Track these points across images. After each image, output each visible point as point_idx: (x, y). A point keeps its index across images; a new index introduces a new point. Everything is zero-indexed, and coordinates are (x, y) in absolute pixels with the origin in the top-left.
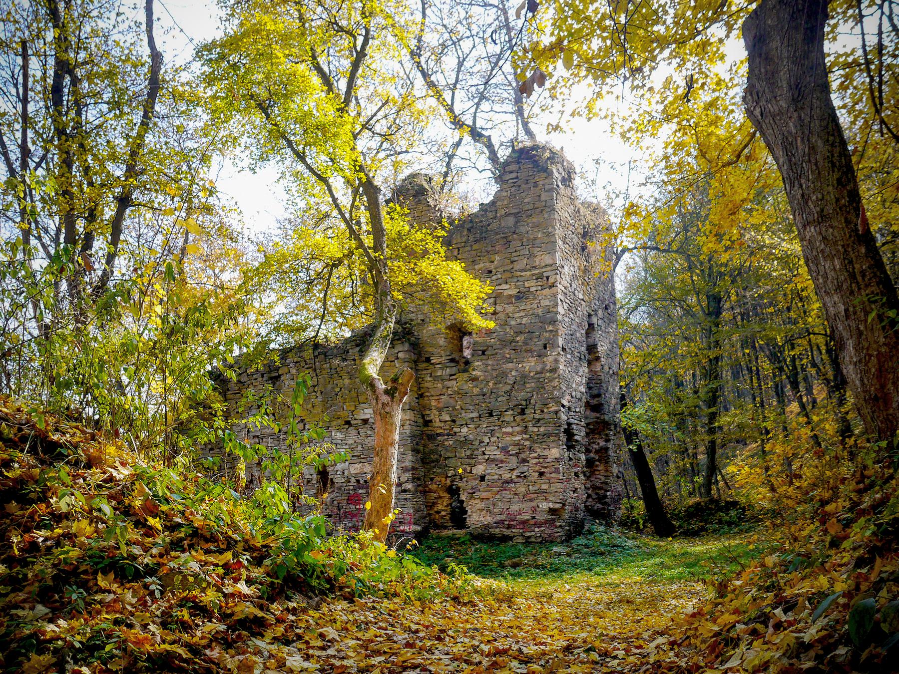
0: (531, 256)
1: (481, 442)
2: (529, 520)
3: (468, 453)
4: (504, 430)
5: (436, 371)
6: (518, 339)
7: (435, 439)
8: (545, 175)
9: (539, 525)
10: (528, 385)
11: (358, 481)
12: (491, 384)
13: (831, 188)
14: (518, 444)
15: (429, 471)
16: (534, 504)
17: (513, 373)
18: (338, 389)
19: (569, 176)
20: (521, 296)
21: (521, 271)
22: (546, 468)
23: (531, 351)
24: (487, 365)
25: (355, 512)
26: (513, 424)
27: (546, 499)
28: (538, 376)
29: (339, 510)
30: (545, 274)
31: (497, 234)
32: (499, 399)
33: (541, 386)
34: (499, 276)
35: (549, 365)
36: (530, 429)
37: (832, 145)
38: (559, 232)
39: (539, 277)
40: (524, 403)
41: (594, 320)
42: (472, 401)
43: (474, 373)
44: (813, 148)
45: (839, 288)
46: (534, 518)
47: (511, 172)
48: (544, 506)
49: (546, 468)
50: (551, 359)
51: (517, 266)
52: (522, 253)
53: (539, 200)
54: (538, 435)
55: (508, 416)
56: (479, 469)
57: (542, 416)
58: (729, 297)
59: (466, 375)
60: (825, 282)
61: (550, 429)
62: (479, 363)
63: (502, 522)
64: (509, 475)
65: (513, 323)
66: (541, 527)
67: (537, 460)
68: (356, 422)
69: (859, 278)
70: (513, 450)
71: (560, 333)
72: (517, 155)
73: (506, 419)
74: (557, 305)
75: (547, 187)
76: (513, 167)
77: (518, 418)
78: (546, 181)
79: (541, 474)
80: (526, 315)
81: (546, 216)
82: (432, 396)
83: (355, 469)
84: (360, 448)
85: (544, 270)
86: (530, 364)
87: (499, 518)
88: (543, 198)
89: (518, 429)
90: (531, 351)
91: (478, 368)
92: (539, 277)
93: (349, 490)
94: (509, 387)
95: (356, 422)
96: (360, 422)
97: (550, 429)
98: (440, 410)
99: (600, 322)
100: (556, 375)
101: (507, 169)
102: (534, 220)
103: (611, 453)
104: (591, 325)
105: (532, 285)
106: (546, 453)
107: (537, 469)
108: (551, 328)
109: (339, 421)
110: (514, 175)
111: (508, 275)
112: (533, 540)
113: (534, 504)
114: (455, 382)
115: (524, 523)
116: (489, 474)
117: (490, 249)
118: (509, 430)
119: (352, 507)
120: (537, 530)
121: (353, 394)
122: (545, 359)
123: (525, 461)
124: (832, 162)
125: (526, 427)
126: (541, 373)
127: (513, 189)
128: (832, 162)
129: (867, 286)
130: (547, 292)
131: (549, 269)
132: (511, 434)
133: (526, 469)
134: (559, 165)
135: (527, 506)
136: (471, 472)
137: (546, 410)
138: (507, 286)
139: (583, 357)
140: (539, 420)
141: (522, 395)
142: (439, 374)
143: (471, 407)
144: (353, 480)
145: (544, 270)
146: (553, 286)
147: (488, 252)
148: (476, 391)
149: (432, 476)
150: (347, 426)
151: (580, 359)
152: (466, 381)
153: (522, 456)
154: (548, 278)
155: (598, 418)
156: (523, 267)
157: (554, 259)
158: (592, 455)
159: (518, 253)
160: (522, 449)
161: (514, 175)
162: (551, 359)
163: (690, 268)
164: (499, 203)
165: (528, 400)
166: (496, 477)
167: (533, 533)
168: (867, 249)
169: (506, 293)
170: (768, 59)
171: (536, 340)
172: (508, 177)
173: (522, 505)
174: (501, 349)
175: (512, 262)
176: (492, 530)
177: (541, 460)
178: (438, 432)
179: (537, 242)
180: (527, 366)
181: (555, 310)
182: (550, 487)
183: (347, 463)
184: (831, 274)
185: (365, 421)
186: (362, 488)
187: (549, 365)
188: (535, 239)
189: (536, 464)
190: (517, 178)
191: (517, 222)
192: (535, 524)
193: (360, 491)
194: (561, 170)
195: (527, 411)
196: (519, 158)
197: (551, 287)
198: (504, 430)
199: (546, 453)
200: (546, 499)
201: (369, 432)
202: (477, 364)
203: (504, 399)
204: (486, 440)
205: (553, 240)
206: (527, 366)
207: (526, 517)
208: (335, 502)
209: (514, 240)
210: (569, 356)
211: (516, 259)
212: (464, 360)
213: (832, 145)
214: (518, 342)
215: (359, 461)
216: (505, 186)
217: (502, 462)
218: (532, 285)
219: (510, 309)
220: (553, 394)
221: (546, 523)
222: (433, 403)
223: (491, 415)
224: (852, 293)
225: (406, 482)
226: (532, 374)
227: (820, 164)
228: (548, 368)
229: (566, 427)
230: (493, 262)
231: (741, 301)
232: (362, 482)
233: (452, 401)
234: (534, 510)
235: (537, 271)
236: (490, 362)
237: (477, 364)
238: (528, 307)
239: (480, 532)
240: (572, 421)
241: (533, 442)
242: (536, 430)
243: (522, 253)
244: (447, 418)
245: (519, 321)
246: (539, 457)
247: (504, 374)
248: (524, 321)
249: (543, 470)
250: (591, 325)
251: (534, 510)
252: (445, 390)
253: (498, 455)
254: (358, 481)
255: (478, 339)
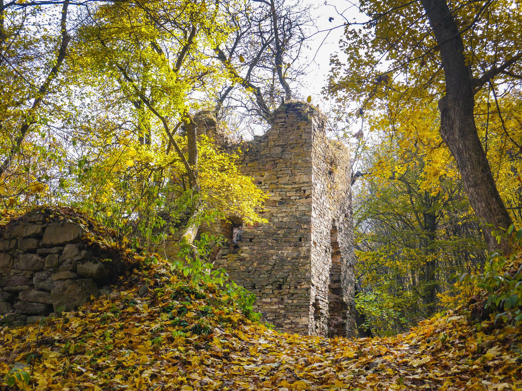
0: (293, 175)
4: (264, 300)
6: (279, 232)
8: (306, 122)
10: (285, 267)
12: (255, 264)
13: (479, 173)
14: (275, 312)
17: (274, 257)
19: (323, 124)
20: (283, 202)
21: (284, 184)
23: (289, 242)
24: (253, 250)
26: (272, 296)
28: (293, 261)
30: (303, 188)
31: (267, 157)
32: (261, 276)
33: (296, 269)
34: (267, 187)
35: (303, 253)
36: (286, 301)
37: (479, 155)
38: (314, 161)
39: (299, 190)
40: (281, 280)
41: (337, 224)
42: (239, 276)
43: (242, 255)
44: (470, 156)
45: (485, 215)
47: (280, 118)
50: (304, 249)
51: (281, 181)
52: (286, 172)
53: (301, 138)
54: (291, 306)
55: (268, 289)
57: (296, 291)
58: (442, 216)
59: (235, 256)
60: (479, 212)
61: (302, 301)
62: (247, 248)
67: (290, 326)
69: (494, 212)
71: (312, 230)
72: (286, 107)
74: (311, 211)
75: (307, 130)
76: (283, 115)
77: (276, 292)
78: (306, 126)
80: (287, 216)
81: (305, 149)
85: (302, 185)
86: (288, 252)
88: (304, 137)
89: (275, 300)
90: (289, 242)
91: (245, 251)
92: (299, 190)
94: (270, 268)
97: (302, 301)
99: (342, 226)
100: (308, 261)
101: (278, 116)
102: (297, 151)
103: (347, 328)
104: (334, 227)
105: (293, 195)
106: (298, 320)
108: (305, 227)
110: (283, 120)
111: (274, 186)
114: (226, 261)
117: (261, 167)
118: (268, 300)
122: (300, 249)
124: (479, 162)
125: (282, 299)
126: (297, 259)
127: (281, 129)
128: (479, 162)
129: (497, 215)
130: (303, 200)
131: (306, 185)
132: (270, 303)
134: (316, 117)
137: (299, 287)
139: (328, 250)
140: (293, 294)
145: (302, 185)
146: (308, 197)
148: (242, 268)
151: (326, 252)
152: (235, 261)
153: (278, 321)
154: (304, 191)
155: (337, 299)
156: (286, 182)
157: (310, 179)
158: (332, 328)
159: (283, 172)
160: (278, 316)
161: (283, 120)
162: (304, 249)
163: (409, 192)
164: (270, 137)
165: (285, 278)
168: (496, 199)
170: (449, 118)
171: (294, 234)
172: (278, 121)
174: (265, 239)
175: (278, 178)
177: (293, 326)
179: (298, 166)
180: (285, 253)
181: (309, 214)
184: (481, 209)
187: (303, 253)
188: (296, 164)
190: (285, 122)
191: (283, 151)
194: (317, 120)
195: (284, 287)
196: (287, 109)
197: (306, 198)
198: (264, 300)
199: (298, 320)
202: (245, 248)
203: (266, 276)
205: (310, 165)
206: (285, 253)
209: (280, 163)
210: (318, 248)
211: (281, 176)
212: (233, 245)
213: (479, 155)
214: (279, 234)
216: (275, 126)
218: (293, 195)
220: (305, 275)
224: (491, 217)
226: (289, 259)
227: (474, 163)
228: (302, 255)
229: (314, 301)
230: (263, 176)
231: (453, 221)
235: (297, 186)
236: (256, 248)
237: (245, 248)
238: (288, 210)
240: (319, 297)
241: (287, 311)
242: (290, 301)
243: (286, 172)
245: (280, 219)
246: (292, 323)
247: (267, 257)
248: (285, 220)
250: (334, 227)
255: (247, 230)
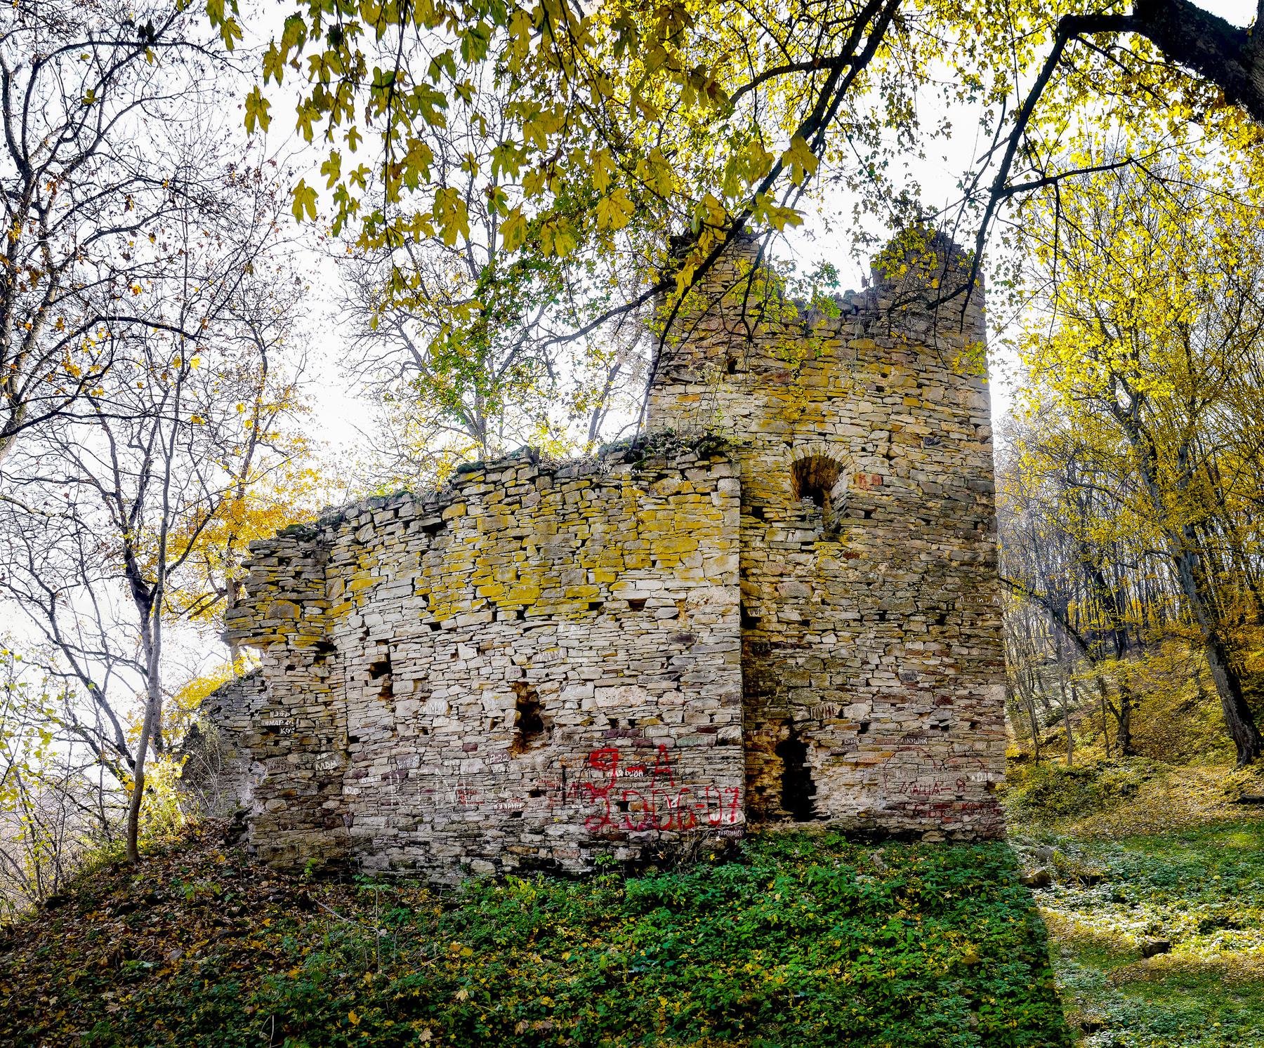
1: (865, 663)
2: (952, 802)
3: (839, 680)
4: (909, 645)
5: (774, 533)
6: (930, 504)
7: (767, 653)
9: (969, 809)
10: (949, 580)
11: (613, 723)
12: (883, 568)
14: (934, 673)
15: (755, 710)
16: (961, 774)
17: (923, 557)
18: (579, 543)
22: (981, 715)
23: (954, 528)
25: (602, 786)
26: (926, 638)
27: (983, 767)
28: (965, 568)
29: (564, 780)
30: (973, 420)
32: (899, 594)
40: (944, 606)
46: (960, 798)
48: (979, 777)
49: (981, 715)
52: (936, 376)
56: (859, 711)
62: (861, 531)
63: (901, 806)
64: (916, 724)
65: (922, 477)
66: (973, 813)
68: (616, 605)
70: (924, 681)
73: (913, 627)
77: (935, 629)
79: (974, 725)
82: (765, 575)
83: (606, 698)
84: (622, 655)
85: (972, 413)
87: (897, 798)
89: (934, 647)
90: (954, 528)
93: (590, 739)
94: (916, 578)
95: (616, 605)
96: (627, 604)
98: (780, 602)
100: (995, 573)
106: (982, 690)
107: (967, 715)
108: (984, 501)
109: (577, 604)
112: (960, 837)
113: (961, 774)
114: (812, 556)
115: (941, 807)
116: (877, 720)
117: (882, 354)
118: (918, 646)
119: (597, 774)
120: (966, 819)
121: (613, 552)
123: (946, 700)
125: (949, 646)
133: (947, 714)
135: (949, 777)
136: (841, 715)
137: (980, 623)
138: (911, 420)
140: (969, 636)
141: (939, 593)
142: (780, 537)
143: (843, 602)
144: (602, 720)
145: (972, 413)
147: (878, 358)
149: (761, 720)
150: (594, 613)
159: (930, 375)
166: (892, 726)
167: (959, 825)
169: (909, 429)
173: (939, 776)
175: (920, 386)
176: (882, 822)
178: (774, 640)
182: (988, 746)
183: (590, 685)
185: (636, 605)
186: (624, 735)
189: (966, 707)
192: (964, 809)
193: (619, 742)
195: (951, 620)
198: (909, 645)
199: (982, 690)
200: (983, 767)
201: (645, 625)
204: (874, 660)
207: (946, 796)
208: (557, 765)
211: (927, 382)
215: (619, 681)
217: (903, 700)
219: (916, 455)
220: (990, 600)
221: (981, 807)
222: (767, 589)
223: (882, 617)
225: (729, 724)
226: (954, 564)
228: (981, 559)
232: (623, 723)
233: (805, 589)
234: (962, 784)
238: (948, 461)
239: (857, 824)
241: (961, 671)
242: (965, 651)
243: (936, 376)
244: (795, 616)
245: (931, 478)
248: (940, 479)
249: (976, 718)
251: (962, 784)
252: (790, 567)
253: (897, 687)
254: (613, 723)
